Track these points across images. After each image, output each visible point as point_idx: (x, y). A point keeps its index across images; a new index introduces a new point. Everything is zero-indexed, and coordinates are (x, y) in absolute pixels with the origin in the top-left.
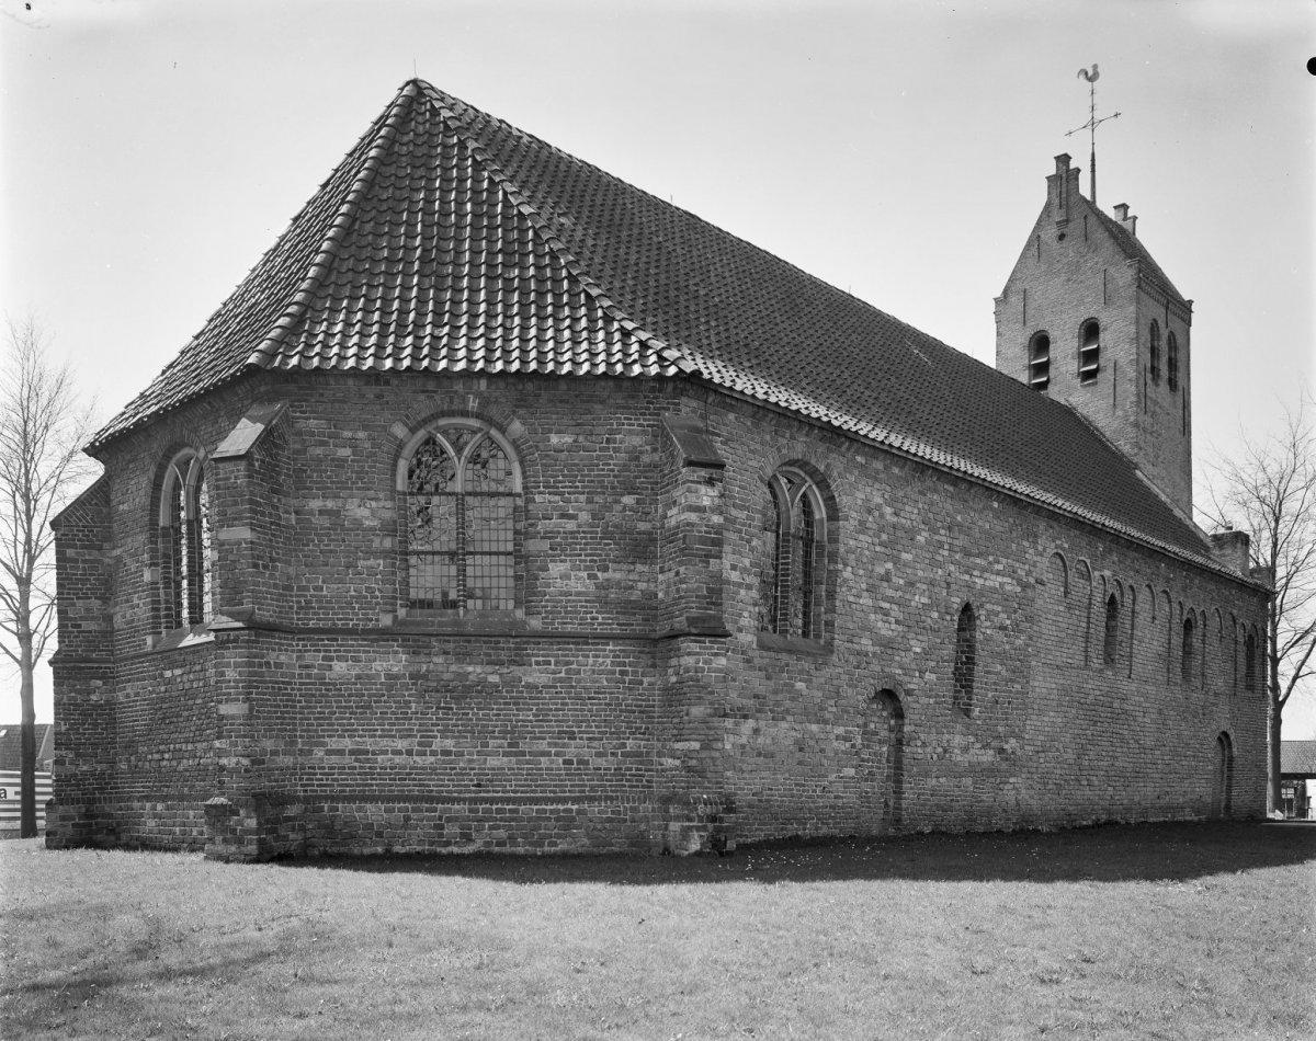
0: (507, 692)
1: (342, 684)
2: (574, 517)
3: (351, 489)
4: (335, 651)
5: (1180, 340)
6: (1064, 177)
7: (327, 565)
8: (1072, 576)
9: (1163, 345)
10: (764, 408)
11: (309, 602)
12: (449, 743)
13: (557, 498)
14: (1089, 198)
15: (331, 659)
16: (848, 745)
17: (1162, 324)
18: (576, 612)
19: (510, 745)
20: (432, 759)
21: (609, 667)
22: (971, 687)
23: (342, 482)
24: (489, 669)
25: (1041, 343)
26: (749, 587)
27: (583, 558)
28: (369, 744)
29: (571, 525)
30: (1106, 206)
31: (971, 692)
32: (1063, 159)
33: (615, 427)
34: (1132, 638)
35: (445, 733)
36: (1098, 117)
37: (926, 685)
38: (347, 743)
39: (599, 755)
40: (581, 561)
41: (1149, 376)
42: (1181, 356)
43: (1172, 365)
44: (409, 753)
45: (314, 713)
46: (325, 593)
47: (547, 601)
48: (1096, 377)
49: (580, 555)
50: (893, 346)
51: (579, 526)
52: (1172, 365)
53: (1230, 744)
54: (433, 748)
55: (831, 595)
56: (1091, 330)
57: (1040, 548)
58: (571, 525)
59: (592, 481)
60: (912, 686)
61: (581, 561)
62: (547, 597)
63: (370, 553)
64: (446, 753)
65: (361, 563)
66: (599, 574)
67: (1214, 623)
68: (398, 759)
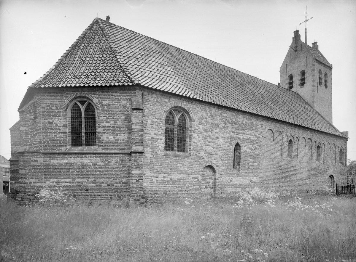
0: (93, 167)
1: (54, 166)
2: (109, 122)
3: (55, 117)
4: (52, 157)
5: (328, 74)
6: (297, 35)
7: (50, 136)
8: (276, 135)
9: (323, 77)
10: (330, 103)
11: (46, 145)
12: (79, 180)
13: (105, 118)
14: (305, 42)
15: (51, 159)
16: (196, 180)
17: (322, 71)
18: (110, 147)
19: (94, 181)
20: (75, 184)
21: (119, 161)
22: (240, 164)
23: (54, 115)
24: (89, 161)
25: (291, 77)
26: (161, 139)
27: (112, 133)
28: (60, 180)
29: (109, 124)
30: (310, 44)
31: (240, 166)
32: (297, 33)
33: (119, 99)
34: (298, 151)
35: (78, 178)
36: (307, 19)
37: (221, 163)
38: (55, 180)
39: (117, 183)
40: (111, 133)
41: (318, 84)
42: (328, 79)
43: (326, 81)
44: (70, 183)
45: (47, 173)
46: (49, 143)
47: (103, 144)
48: (304, 85)
49: (111, 132)
50: (198, 77)
51: (111, 124)
52: (326, 81)
53: (333, 178)
54: (75, 181)
55: (190, 141)
56: (303, 73)
57: (264, 128)
58: (109, 124)
59: (114, 113)
60: (219, 164)
61: (111, 133)
62: (103, 143)
63: (60, 132)
64: (79, 182)
65: (58, 135)
66: (116, 137)
67: (327, 147)
68: (67, 184)
